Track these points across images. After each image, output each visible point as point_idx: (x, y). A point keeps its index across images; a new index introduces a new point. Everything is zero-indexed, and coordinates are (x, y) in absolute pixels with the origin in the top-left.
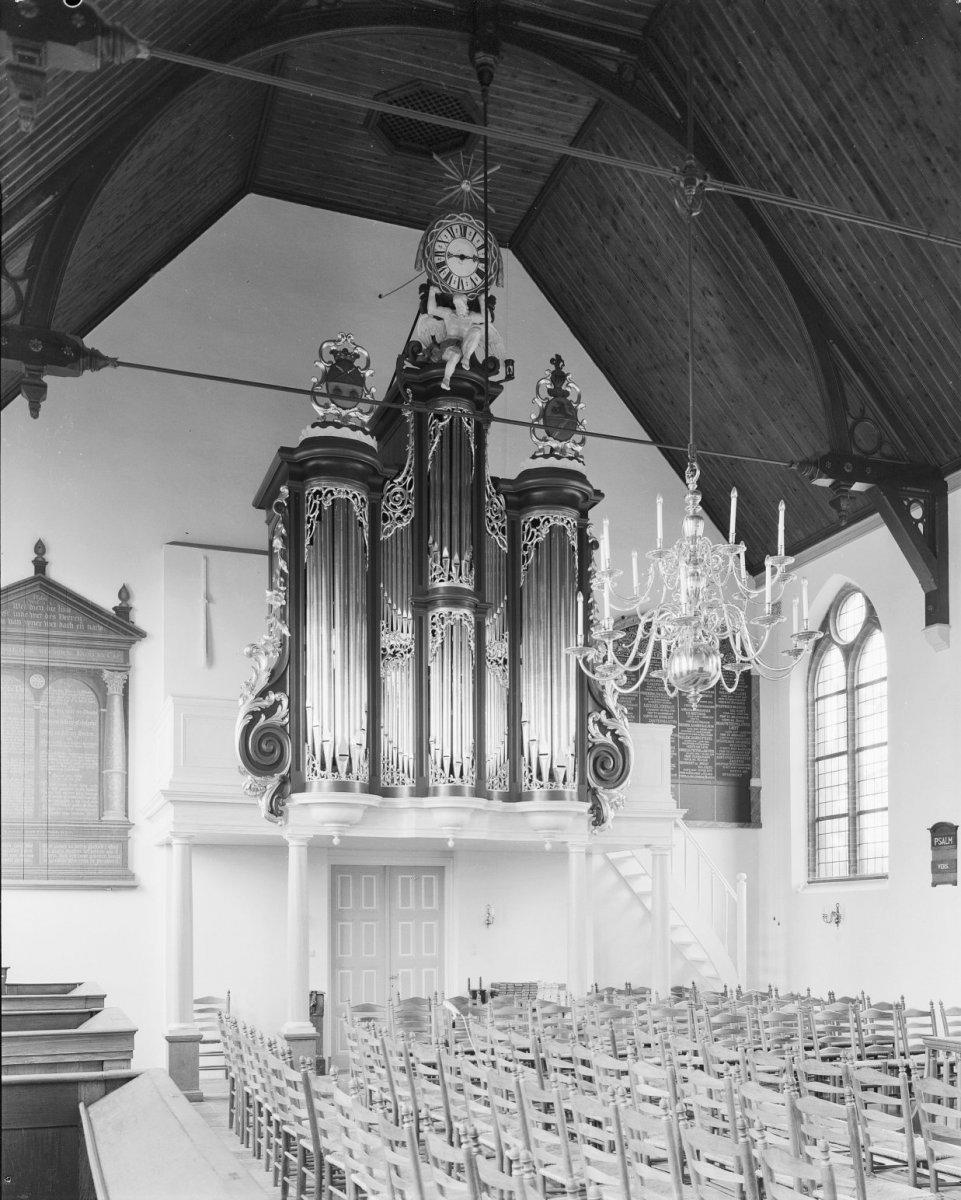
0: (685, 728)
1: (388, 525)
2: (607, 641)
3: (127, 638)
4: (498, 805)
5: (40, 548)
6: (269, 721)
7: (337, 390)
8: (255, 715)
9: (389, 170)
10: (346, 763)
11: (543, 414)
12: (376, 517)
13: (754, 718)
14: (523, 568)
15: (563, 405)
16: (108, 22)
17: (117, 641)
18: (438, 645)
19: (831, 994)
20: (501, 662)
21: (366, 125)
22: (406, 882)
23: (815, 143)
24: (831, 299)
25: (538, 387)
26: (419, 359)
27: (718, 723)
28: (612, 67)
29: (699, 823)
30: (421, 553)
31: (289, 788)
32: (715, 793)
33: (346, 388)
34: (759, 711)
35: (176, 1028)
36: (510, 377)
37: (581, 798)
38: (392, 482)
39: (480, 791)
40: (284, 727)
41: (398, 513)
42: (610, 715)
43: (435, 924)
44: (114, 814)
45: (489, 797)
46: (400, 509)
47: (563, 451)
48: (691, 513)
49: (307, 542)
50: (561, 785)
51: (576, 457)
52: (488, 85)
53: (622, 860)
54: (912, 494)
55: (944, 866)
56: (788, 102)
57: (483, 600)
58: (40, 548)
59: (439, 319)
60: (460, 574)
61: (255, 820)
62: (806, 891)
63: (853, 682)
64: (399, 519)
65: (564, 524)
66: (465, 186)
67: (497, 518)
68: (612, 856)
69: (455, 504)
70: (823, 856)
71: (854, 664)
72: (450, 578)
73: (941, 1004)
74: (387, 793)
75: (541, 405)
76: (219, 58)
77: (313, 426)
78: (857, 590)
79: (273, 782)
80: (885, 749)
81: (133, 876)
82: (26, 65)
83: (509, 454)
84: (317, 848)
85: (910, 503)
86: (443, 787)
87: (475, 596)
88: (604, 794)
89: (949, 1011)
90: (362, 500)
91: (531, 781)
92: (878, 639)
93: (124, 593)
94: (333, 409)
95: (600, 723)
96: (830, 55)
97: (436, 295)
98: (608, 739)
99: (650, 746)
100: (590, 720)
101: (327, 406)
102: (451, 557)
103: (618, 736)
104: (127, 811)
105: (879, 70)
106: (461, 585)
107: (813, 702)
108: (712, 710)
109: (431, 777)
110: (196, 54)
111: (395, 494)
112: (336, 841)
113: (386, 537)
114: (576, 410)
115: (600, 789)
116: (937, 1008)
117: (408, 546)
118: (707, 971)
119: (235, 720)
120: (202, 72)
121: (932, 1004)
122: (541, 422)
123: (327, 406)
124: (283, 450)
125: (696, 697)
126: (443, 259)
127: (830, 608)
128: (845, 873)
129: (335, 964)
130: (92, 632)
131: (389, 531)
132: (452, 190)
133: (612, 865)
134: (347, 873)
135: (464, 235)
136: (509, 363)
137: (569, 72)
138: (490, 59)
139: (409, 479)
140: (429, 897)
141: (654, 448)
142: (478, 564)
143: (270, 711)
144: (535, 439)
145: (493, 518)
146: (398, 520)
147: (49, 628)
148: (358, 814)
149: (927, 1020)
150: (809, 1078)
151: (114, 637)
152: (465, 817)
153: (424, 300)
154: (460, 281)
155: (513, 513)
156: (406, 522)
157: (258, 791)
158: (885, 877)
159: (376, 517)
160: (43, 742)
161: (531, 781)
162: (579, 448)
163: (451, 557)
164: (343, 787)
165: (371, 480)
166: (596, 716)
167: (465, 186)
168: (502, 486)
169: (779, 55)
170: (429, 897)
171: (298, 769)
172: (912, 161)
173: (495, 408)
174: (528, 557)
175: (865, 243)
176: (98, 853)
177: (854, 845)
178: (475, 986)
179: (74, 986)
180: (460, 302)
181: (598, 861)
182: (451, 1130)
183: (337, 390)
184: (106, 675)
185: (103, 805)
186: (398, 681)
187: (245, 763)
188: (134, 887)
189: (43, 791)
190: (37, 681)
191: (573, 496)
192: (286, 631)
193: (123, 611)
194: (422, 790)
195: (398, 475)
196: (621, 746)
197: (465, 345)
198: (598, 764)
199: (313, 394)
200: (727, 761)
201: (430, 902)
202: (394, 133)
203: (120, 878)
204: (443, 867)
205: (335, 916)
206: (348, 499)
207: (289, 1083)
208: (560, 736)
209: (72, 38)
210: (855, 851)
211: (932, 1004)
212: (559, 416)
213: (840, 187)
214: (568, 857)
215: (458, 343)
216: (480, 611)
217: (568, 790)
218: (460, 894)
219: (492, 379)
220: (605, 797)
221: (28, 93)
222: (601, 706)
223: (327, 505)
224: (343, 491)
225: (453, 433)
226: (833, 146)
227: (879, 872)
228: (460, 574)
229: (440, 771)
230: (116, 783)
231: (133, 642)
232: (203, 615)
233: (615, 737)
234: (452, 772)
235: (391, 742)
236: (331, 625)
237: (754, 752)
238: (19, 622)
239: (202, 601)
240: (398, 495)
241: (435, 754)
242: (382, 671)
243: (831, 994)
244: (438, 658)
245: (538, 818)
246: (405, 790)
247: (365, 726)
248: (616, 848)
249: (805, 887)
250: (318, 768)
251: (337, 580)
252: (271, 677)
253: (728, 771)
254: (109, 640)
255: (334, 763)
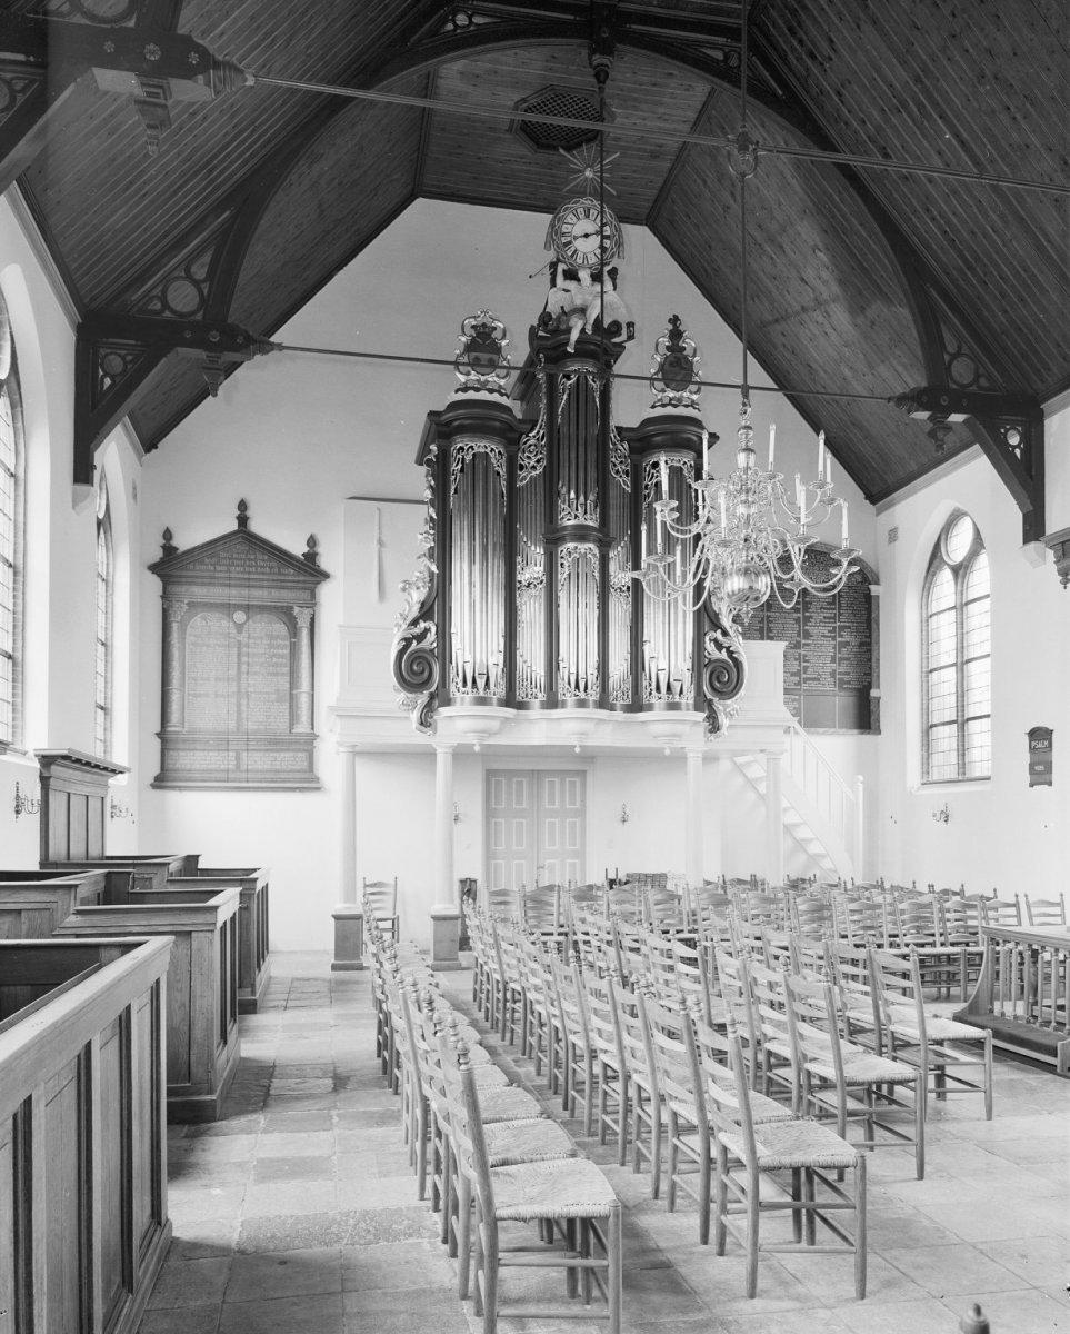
0: (808, 645)
1: (523, 474)
2: (659, 564)
3: (314, 579)
4: (619, 715)
5: (243, 506)
6: (420, 646)
7: (477, 358)
8: (408, 641)
9: (531, 163)
10: (484, 681)
11: (662, 368)
12: (513, 467)
13: (874, 637)
14: (645, 505)
15: (679, 359)
16: (220, 58)
17: (304, 582)
18: (565, 576)
19: (931, 886)
20: (625, 589)
21: (510, 130)
22: (552, 784)
23: (904, 105)
24: (928, 247)
25: (657, 345)
26: (550, 327)
27: (838, 639)
28: (719, 55)
29: (821, 730)
30: (551, 497)
31: (436, 703)
32: (840, 702)
33: (484, 357)
34: (878, 629)
35: (342, 908)
36: (631, 337)
37: (697, 708)
38: (527, 436)
39: (604, 703)
40: (432, 651)
41: (532, 463)
42: (725, 633)
43: (578, 821)
44: (302, 727)
45: (612, 709)
46: (534, 459)
47: (680, 400)
48: (744, 447)
49: (453, 492)
50: (677, 697)
51: (693, 404)
52: (604, 83)
53: (749, 764)
54: (1007, 422)
55: (1040, 768)
56: (878, 70)
57: (607, 535)
58: (243, 506)
59: (567, 291)
60: (586, 513)
61: (404, 728)
62: (920, 792)
63: (962, 599)
64: (534, 467)
65: (681, 465)
66: (589, 173)
67: (621, 462)
68: (740, 760)
69: (581, 449)
70: (936, 759)
71: (963, 582)
72: (576, 516)
73: (1026, 896)
74: (521, 706)
75: (659, 360)
76: (365, 86)
77: (457, 391)
78: (965, 514)
79: (423, 698)
80: (988, 660)
81: (317, 780)
82: (152, 100)
83: (631, 406)
84: (461, 755)
85: (1007, 431)
86: (570, 700)
87: (601, 532)
88: (719, 705)
89: (1035, 903)
90: (500, 452)
91: (650, 694)
92: (983, 560)
93: (312, 542)
94: (474, 376)
95: (716, 641)
96: (913, 22)
97: (564, 271)
98: (724, 655)
99: (764, 661)
100: (707, 638)
101: (468, 374)
102: (577, 498)
103: (733, 652)
104: (313, 724)
105: (958, 31)
106: (587, 523)
107: (926, 620)
108: (834, 628)
109: (560, 691)
110: (346, 85)
111: (530, 446)
112: (477, 748)
113: (521, 484)
114: (692, 363)
115: (716, 700)
116: (1022, 901)
117: (540, 490)
118: (827, 864)
119: (391, 645)
120: (349, 99)
121: (1017, 896)
122: (660, 376)
123: (468, 374)
124: (432, 414)
125: (747, 613)
126: (569, 239)
127: (942, 530)
128: (954, 776)
129: (489, 856)
130: (285, 575)
131: (524, 478)
132: (576, 178)
133: (739, 768)
134: (502, 776)
135: (587, 216)
136: (630, 325)
137: (678, 63)
138: (605, 60)
139: (542, 432)
140: (573, 795)
141: (780, 394)
142: (603, 503)
143: (421, 637)
144: (654, 391)
145: (617, 462)
146: (533, 466)
147: (249, 573)
148: (495, 725)
149: (1012, 911)
150: (843, 961)
151: (302, 578)
152: (589, 726)
153: (554, 275)
154: (585, 257)
155: (635, 457)
156: (539, 470)
157: (410, 706)
158: (989, 779)
159: (513, 467)
160: (244, 668)
161: (650, 694)
162: (695, 397)
163: (577, 498)
164: (482, 701)
165: (509, 435)
166: (712, 634)
167: (589, 173)
168: (624, 434)
169: (867, 28)
170: (573, 795)
171: (444, 686)
172: (993, 111)
173: (618, 368)
174: (649, 495)
175: (955, 192)
176: (289, 760)
177: (962, 750)
178: (612, 876)
179: (254, 870)
180: (584, 275)
181: (725, 765)
182: (525, 1000)
183: (477, 358)
184: (296, 610)
185: (293, 718)
186: (531, 610)
187: (399, 682)
188: (318, 789)
189: (244, 708)
190: (240, 616)
191: (690, 440)
192: (434, 568)
193: (311, 557)
194: (552, 702)
195: (532, 430)
196: (735, 660)
197: (588, 313)
198: (714, 676)
199: (456, 364)
200: (848, 674)
201: (573, 802)
202: (539, 137)
203: (307, 781)
204: (585, 772)
205: (490, 813)
206: (487, 453)
207: (529, 955)
208: (676, 654)
209: (189, 73)
210: (964, 755)
211: (1017, 896)
212: (677, 368)
213: (929, 142)
214: (686, 762)
215: (582, 311)
216: (605, 545)
217: (684, 701)
218: (601, 799)
219: (616, 340)
220: (721, 708)
221: (152, 122)
222: (716, 625)
223: (468, 458)
224: (482, 445)
225: (580, 390)
226: (920, 106)
227: (986, 774)
228: (586, 513)
229: (567, 686)
230: (304, 700)
231: (319, 583)
232: (376, 559)
233: (730, 653)
234: (577, 687)
235: (525, 662)
236: (472, 562)
237: (874, 665)
238: (225, 568)
239: (375, 547)
240: (533, 447)
241: (563, 672)
242: (518, 601)
243: (931, 886)
244: (565, 587)
245: (661, 727)
246: (536, 703)
247: (502, 648)
248: (743, 753)
249: (918, 789)
250: (460, 684)
251: (477, 522)
252: (421, 608)
253: (849, 683)
254: (298, 581)
255: (474, 682)
